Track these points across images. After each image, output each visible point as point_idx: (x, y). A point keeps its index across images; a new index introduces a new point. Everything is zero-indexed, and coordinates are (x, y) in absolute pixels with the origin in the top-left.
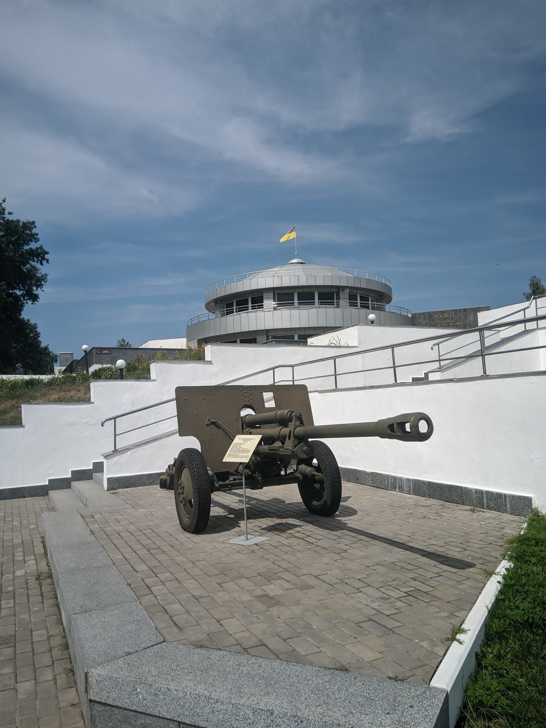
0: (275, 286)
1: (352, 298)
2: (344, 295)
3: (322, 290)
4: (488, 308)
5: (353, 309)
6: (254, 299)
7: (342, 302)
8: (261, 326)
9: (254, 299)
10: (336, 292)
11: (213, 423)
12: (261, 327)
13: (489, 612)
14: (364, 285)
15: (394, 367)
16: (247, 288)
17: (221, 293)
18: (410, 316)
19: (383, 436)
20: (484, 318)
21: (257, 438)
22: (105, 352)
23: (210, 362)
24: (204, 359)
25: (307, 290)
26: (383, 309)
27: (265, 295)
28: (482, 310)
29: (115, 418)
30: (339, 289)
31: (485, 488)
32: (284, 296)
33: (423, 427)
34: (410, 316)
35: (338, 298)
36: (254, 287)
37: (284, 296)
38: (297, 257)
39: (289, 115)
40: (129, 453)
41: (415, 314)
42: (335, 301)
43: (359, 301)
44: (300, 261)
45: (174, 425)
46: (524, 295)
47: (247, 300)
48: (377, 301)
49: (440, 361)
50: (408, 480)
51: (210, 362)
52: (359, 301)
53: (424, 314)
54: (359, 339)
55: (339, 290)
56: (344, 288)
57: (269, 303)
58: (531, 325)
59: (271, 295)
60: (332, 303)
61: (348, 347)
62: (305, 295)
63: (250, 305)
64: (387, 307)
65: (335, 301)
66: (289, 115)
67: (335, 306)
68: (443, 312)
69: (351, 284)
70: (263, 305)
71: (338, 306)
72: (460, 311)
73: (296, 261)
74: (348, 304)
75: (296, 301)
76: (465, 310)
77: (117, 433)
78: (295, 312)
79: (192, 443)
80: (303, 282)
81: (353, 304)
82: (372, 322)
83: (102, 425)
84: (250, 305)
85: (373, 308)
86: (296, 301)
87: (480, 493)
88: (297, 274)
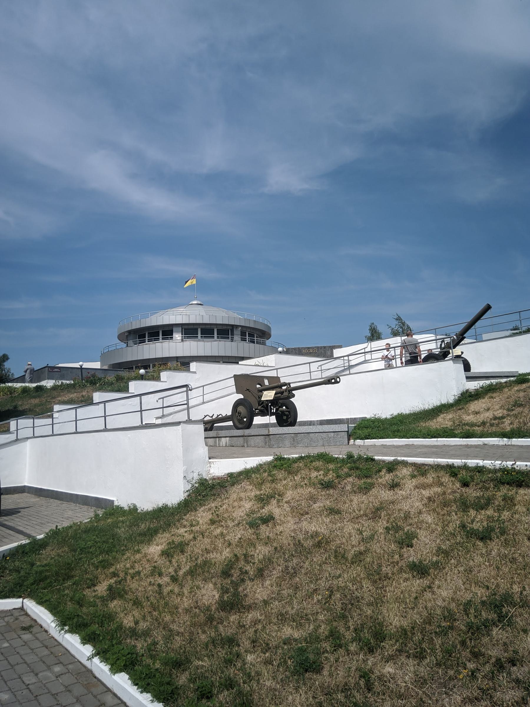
0: (184, 322)
1: (243, 334)
2: (237, 332)
3: (220, 328)
4: (340, 347)
5: (252, 345)
6: (167, 332)
8: (173, 354)
9: (167, 332)
11: (248, 390)
14: (252, 325)
16: (160, 323)
17: (136, 325)
19: (325, 384)
20: (337, 353)
21: (274, 392)
22: (56, 370)
23: (195, 372)
24: (190, 370)
25: (209, 327)
26: (264, 344)
27: (174, 329)
28: (336, 348)
31: (349, 417)
32: (190, 331)
33: (338, 380)
35: (232, 334)
37: (190, 331)
38: (196, 299)
39: (154, 154)
40: (172, 416)
41: (288, 349)
42: (230, 336)
43: (247, 337)
45: (234, 389)
46: (366, 337)
48: (261, 337)
50: (317, 421)
51: (195, 372)
52: (247, 337)
54: (276, 363)
55: (233, 328)
56: (237, 326)
57: (177, 336)
58: (368, 357)
60: (228, 338)
61: (268, 366)
62: (207, 331)
63: (161, 337)
66: (154, 154)
67: (230, 340)
68: (309, 348)
69: (243, 324)
71: (232, 340)
72: (321, 348)
74: (240, 339)
75: (199, 335)
76: (325, 347)
78: (201, 344)
79: (241, 396)
80: (206, 321)
81: (244, 340)
82: (280, 352)
84: (161, 337)
85: (257, 343)
86: (199, 335)
87: (348, 419)
88: (201, 314)
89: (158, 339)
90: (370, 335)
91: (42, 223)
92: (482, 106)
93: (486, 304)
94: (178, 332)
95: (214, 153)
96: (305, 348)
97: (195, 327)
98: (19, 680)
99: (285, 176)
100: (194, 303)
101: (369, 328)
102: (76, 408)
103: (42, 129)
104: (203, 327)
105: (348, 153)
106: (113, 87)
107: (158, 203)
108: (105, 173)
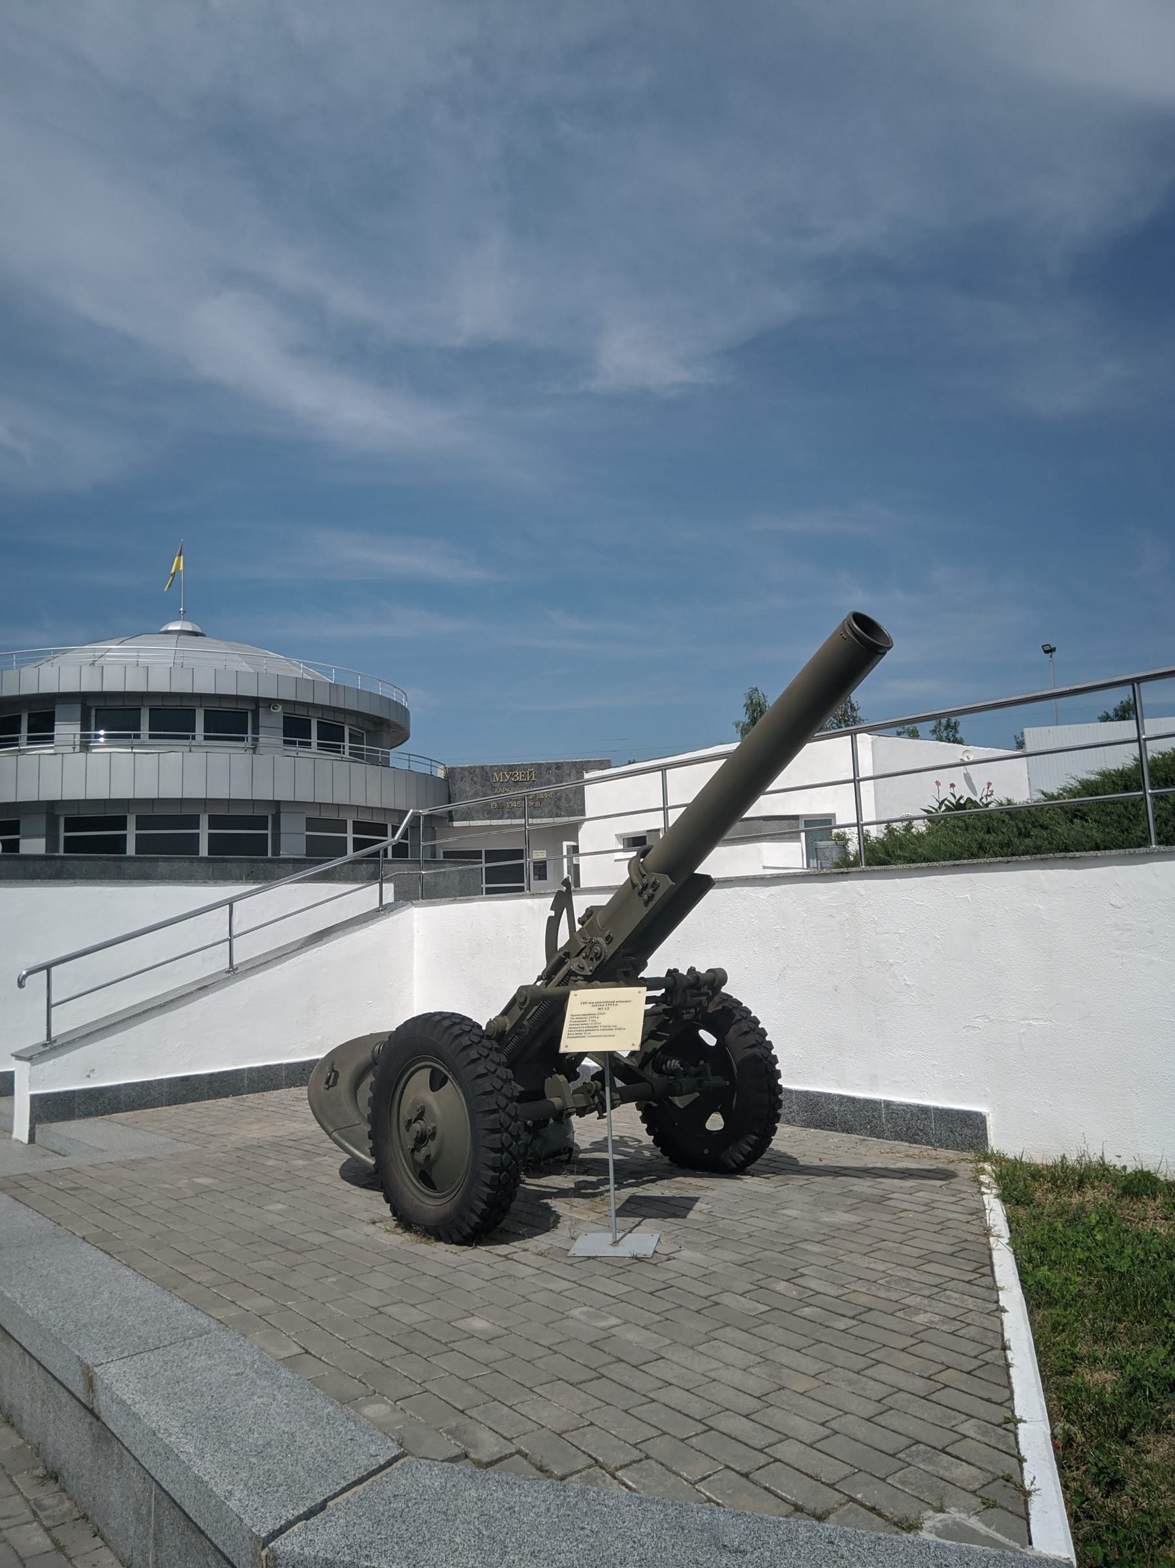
0: (128, 690)
2: (272, 721)
3: (214, 706)
7: (263, 739)
10: (252, 711)
12: (28, 794)
13: (645, 1217)
14: (322, 699)
15: (856, 781)
18: (441, 774)
25: (175, 703)
27: (59, 710)
29: (48, 967)
30: (258, 704)
34: (441, 774)
35: (256, 730)
36: (29, 687)
38: (185, 616)
39: (350, 301)
44: (189, 627)
46: (737, 726)
47: (19, 718)
49: (856, 781)
53: (471, 770)
55: (258, 707)
56: (271, 702)
57: (67, 731)
59: (77, 709)
64: (397, 757)
65: (250, 735)
66: (350, 301)
68: (511, 768)
70: (52, 737)
72: (549, 767)
73: (178, 628)
75: (145, 731)
76: (559, 766)
77: (53, 1002)
83: (21, 984)
86: (145, 731)
89: (14, 742)
90: (746, 719)
91: (93, 456)
92: (1077, 202)
93: (844, 614)
94: (68, 719)
95: (482, 298)
96: (499, 769)
97: (130, 704)
98: (18, 1497)
99: (639, 353)
100: (171, 628)
101: (745, 701)
102: (663, 769)
103: (96, 242)
104: (157, 703)
105: (782, 304)
106: (252, 151)
107: (355, 413)
108: (237, 344)
